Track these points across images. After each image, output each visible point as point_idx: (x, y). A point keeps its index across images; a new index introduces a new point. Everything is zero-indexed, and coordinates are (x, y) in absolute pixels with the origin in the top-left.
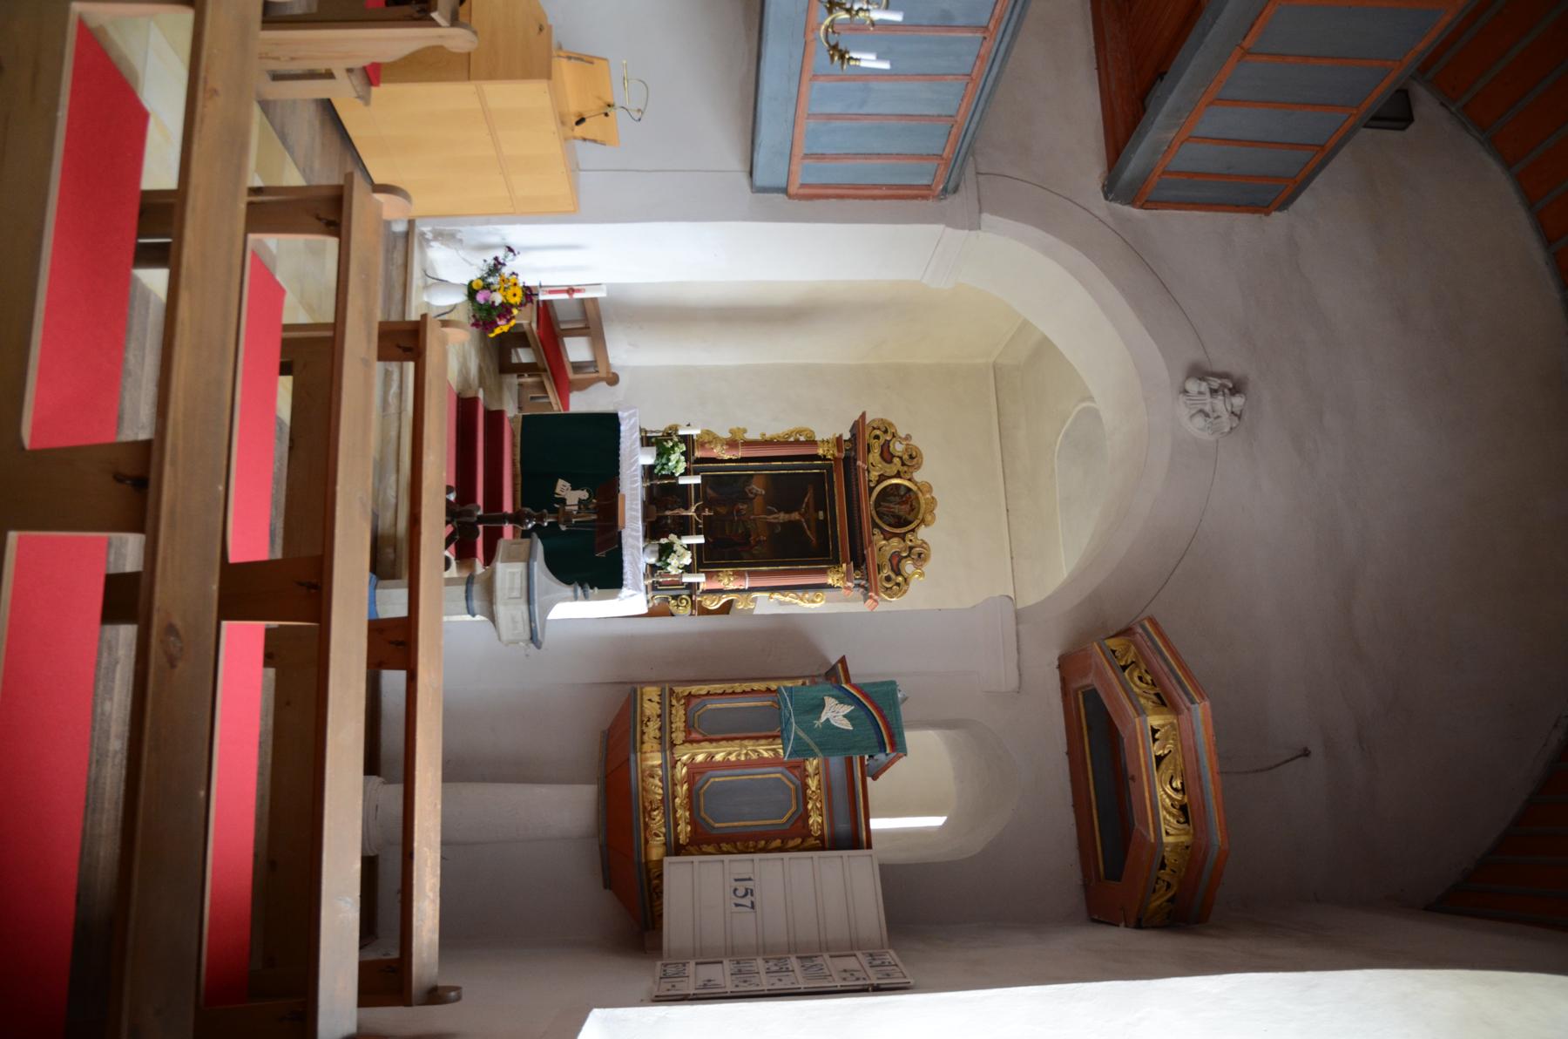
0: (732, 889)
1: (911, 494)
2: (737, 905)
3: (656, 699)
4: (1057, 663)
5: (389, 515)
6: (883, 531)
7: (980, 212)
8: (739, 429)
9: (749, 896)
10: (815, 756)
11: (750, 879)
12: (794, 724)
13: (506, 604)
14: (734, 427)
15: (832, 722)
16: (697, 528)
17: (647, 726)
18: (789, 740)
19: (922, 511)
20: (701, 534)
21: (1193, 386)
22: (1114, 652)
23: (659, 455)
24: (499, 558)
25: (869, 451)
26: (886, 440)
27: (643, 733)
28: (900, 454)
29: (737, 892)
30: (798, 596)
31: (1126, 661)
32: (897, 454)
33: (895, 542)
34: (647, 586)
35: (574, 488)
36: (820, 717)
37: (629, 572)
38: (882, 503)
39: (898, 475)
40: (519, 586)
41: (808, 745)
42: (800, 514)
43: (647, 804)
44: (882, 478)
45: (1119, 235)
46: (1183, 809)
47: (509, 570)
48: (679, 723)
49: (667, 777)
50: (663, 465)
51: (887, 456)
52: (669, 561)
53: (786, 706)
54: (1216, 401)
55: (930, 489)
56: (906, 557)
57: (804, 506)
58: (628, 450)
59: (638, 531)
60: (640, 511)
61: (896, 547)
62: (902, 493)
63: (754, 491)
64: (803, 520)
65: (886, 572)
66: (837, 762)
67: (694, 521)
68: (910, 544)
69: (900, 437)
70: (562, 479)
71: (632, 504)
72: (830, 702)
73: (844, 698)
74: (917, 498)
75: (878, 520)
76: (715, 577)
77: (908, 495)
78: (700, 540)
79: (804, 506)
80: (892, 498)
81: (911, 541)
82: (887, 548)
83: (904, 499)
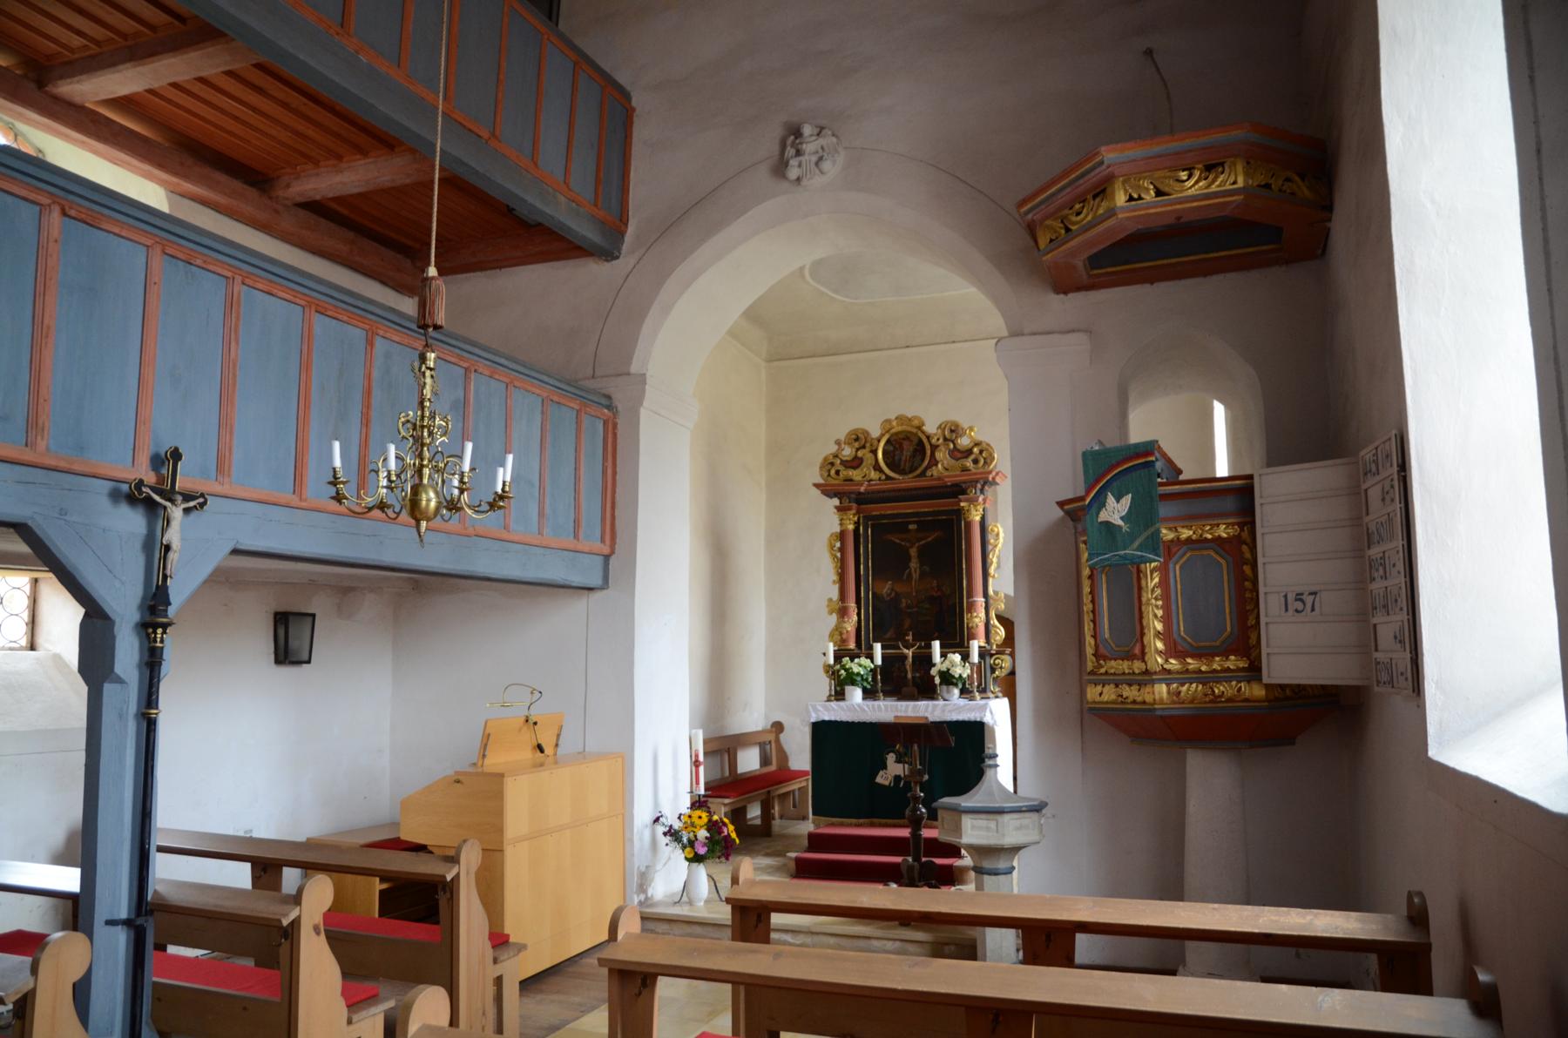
1: (892, 439)
2: (1313, 610)
3: (1099, 688)
4: (1062, 296)
7: (628, 374)
9: (1304, 597)
10: (1158, 531)
11: (1286, 596)
13: (1003, 835)
15: (1124, 514)
18: (1142, 556)
19: (909, 429)
21: (793, 173)
22: (1051, 241)
23: (853, 683)
24: (958, 840)
25: (851, 480)
26: (841, 464)
27: (1134, 702)
28: (854, 450)
29: (1300, 608)
31: (1061, 228)
33: (939, 455)
35: (885, 767)
39: (874, 452)
40: (985, 822)
41: (1148, 538)
42: (911, 547)
44: (877, 467)
46: (1209, 168)
47: (969, 831)
48: (1124, 666)
51: (855, 463)
52: (957, 676)
53: (1105, 559)
54: (808, 151)
55: (888, 421)
57: (903, 543)
59: (928, 705)
62: (891, 448)
64: (917, 545)
65: (969, 463)
66: (1165, 510)
67: (918, 651)
68: (941, 441)
70: (875, 778)
72: (1104, 516)
73: (1099, 501)
75: (918, 472)
77: (894, 443)
78: (936, 645)
79: (903, 543)
80: (897, 458)
81: (938, 439)
82: (945, 462)
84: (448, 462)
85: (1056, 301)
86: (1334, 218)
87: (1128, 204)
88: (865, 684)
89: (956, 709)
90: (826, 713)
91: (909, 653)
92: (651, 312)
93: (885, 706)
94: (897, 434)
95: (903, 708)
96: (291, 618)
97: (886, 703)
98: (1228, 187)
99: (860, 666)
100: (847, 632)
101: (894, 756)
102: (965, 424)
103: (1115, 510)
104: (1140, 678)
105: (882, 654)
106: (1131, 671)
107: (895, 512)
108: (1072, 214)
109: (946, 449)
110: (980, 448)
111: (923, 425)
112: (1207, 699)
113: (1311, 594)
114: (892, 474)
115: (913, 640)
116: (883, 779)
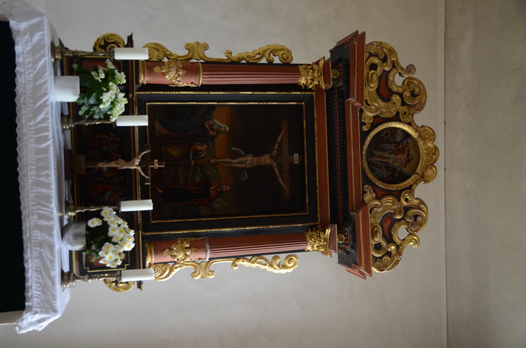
1: (409, 141)
6: (375, 188)
8: (198, 43)
14: (192, 41)
20: (148, 198)
23: (85, 91)
26: (384, 71)
28: (400, 90)
30: (266, 260)
32: (395, 89)
33: (389, 201)
34: (71, 252)
37: (34, 287)
38: (374, 152)
39: (397, 118)
42: (271, 157)
50: (91, 106)
52: (101, 253)
55: (433, 136)
56: (399, 220)
58: (30, 87)
62: (399, 139)
63: (216, 127)
64: (275, 164)
65: (378, 239)
67: (138, 177)
68: (405, 204)
71: (39, 176)
74: (416, 145)
75: (370, 176)
77: (405, 142)
78: (147, 206)
81: (407, 200)
82: (380, 210)
83: (401, 147)
88: (84, 109)
93: (48, 146)
100: (164, 74)
102: (421, 234)
105: (133, 127)
109: (395, 211)
110: (394, 253)
111: (426, 181)
114: (369, 139)
115: (152, 168)
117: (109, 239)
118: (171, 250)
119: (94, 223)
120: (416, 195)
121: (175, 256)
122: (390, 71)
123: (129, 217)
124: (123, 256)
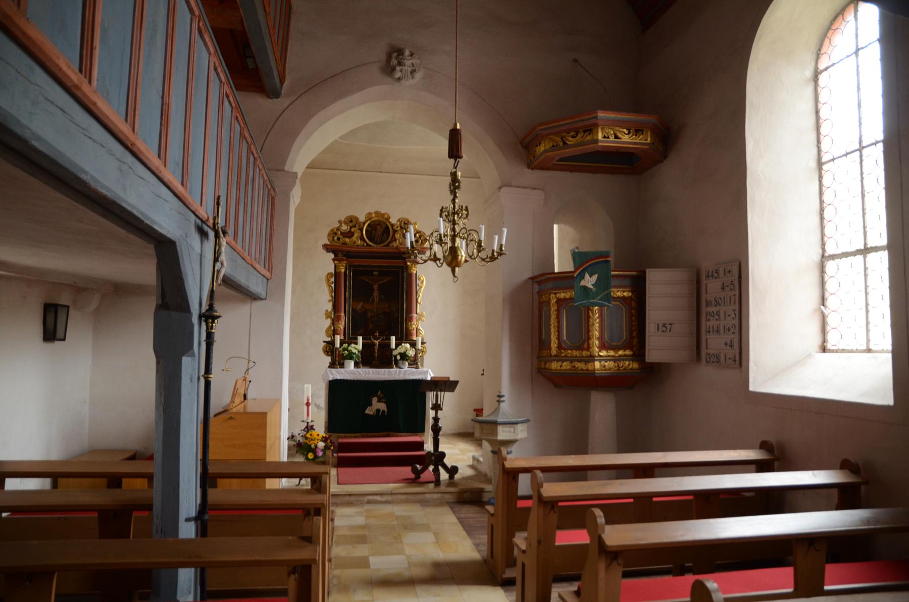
0: (663, 333)
2: (670, 331)
3: (560, 363)
4: (531, 170)
5: (446, 496)
6: (391, 242)
7: (284, 171)
9: (666, 326)
11: (658, 325)
12: (594, 301)
13: (517, 435)
15: (593, 283)
16: (386, 339)
17: (578, 368)
18: (602, 303)
19: (382, 219)
21: (398, 74)
22: (553, 146)
23: (351, 358)
24: (495, 438)
25: (346, 244)
26: (341, 234)
27: (582, 370)
28: (349, 227)
29: (664, 330)
30: (419, 289)
32: (349, 230)
33: (397, 236)
35: (371, 404)
36: (591, 289)
39: (361, 230)
43: (573, 369)
44: (362, 238)
45: (301, 95)
47: (501, 434)
49: (605, 360)
51: (350, 234)
52: (410, 356)
53: (584, 303)
54: (407, 64)
55: (370, 214)
57: (370, 282)
58: (351, 375)
59: (396, 371)
60: (385, 370)
61: (400, 236)
62: (370, 229)
64: (378, 283)
66: (614, 282)
68: (399, 228)
69: (340, 226)
70: (365, 411)
72: (583, 283)
73: (581, 276)
75: (386, 243)
76: (411, 332)
78: (393, 338)
79: (370, 282)
80: (373, 234)
81: (397, 227)
82: (401, 240)
84: (470, 234)
85: (528, 172)
86: (665, 162)
87: (603, 139)
89: (412, 373)
90: (338, 375)
91: (377, 342)
92: (300, 135)
94: (374, 221)
95: (383, 373)
96: (59, 308)
97: (363, 369)
98: (643, 141)
99: (356, 349)
101: (377, 399)
103: (589, 281)
104: (586, 359)
105: (363, 342)
106: (581, 355)
107: (368, 264)
108: (569, 136)
111: (390, 218)
112: (616, 369)
113: (670, 324)
116: (369, 411)
117: (405, 353)
118: (411, 330)
119: (398, 357)
120: (396, 223)
121: (414, 329)
122: (340, 231)
123: (397, 345)
124: (412, 348)
